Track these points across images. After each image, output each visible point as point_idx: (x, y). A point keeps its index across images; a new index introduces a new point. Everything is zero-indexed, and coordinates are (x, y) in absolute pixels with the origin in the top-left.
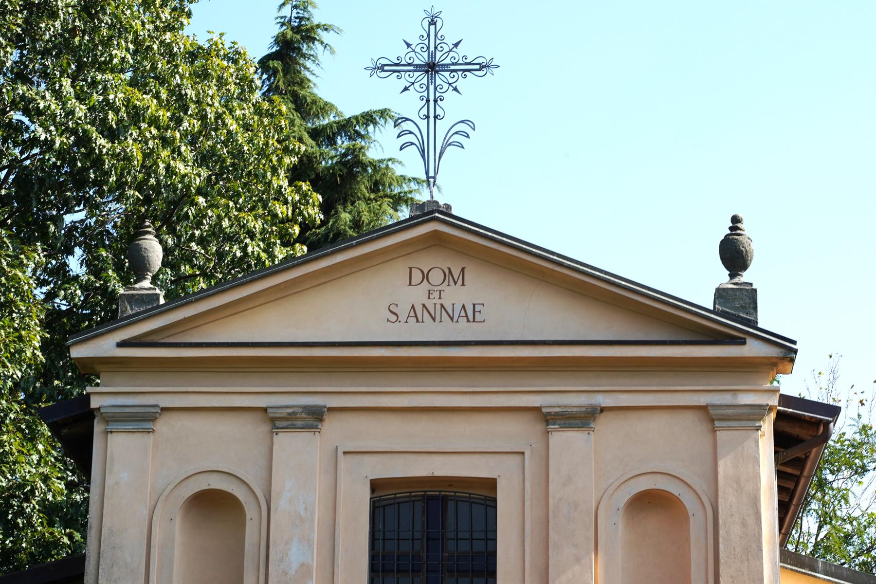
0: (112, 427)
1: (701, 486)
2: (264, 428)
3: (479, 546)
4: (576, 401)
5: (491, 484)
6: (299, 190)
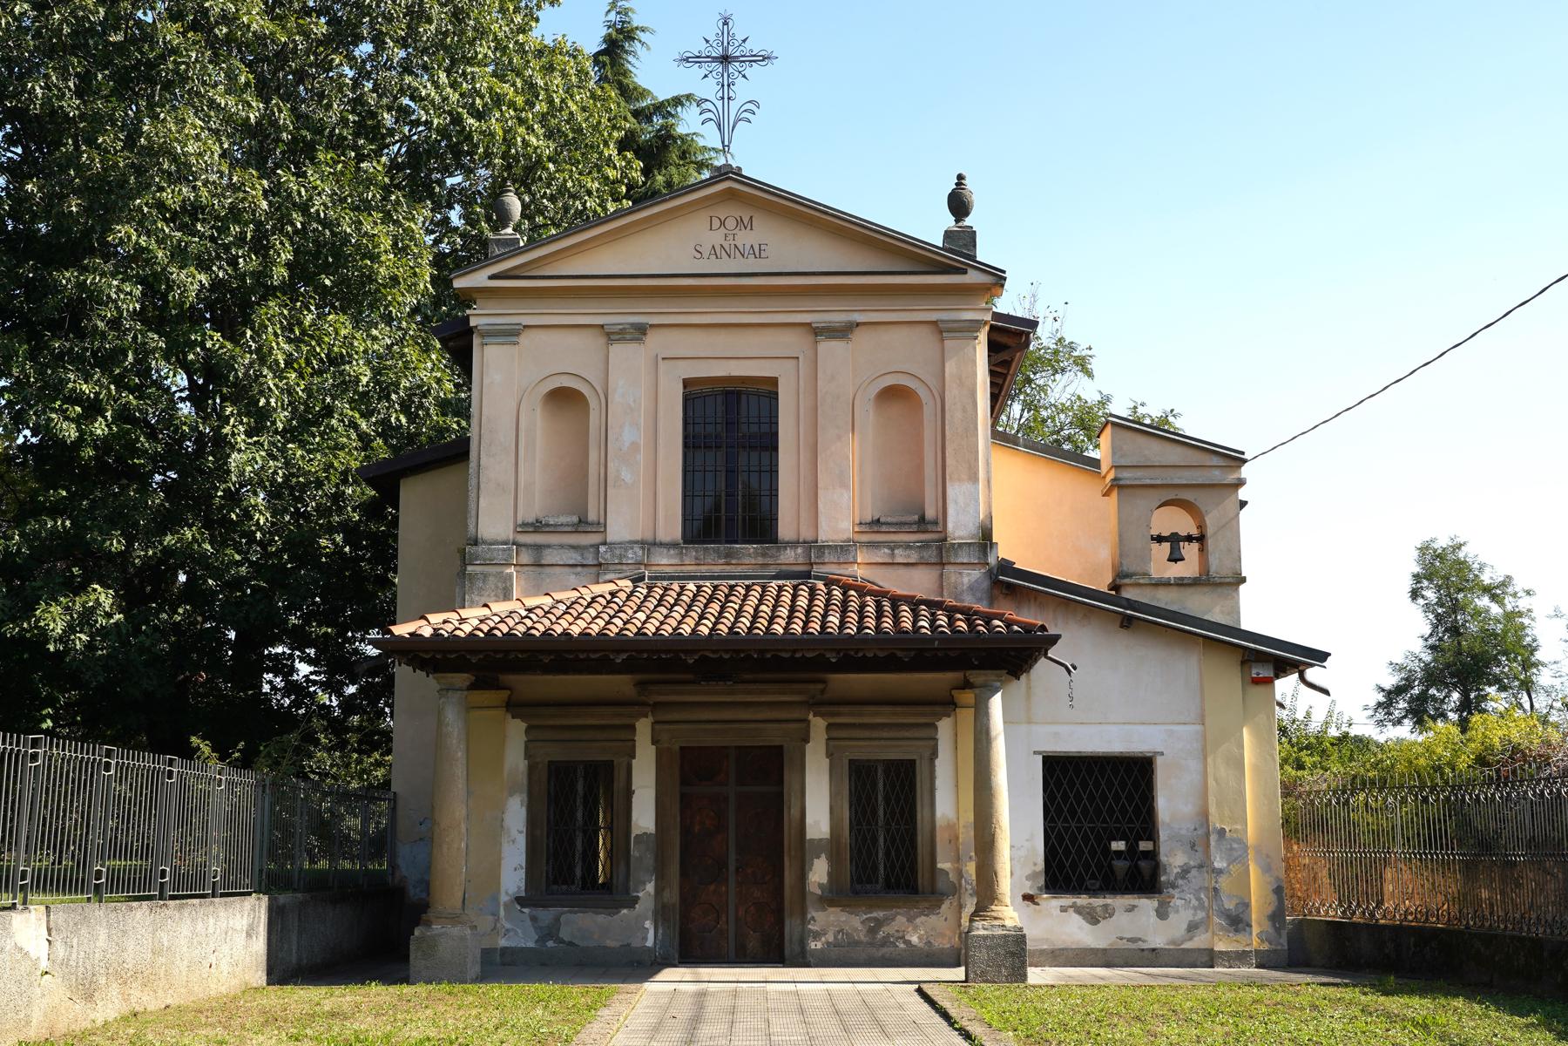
1: (932, 382)
3: (765, 428)
5: (774, 381)
6: (625, 158)
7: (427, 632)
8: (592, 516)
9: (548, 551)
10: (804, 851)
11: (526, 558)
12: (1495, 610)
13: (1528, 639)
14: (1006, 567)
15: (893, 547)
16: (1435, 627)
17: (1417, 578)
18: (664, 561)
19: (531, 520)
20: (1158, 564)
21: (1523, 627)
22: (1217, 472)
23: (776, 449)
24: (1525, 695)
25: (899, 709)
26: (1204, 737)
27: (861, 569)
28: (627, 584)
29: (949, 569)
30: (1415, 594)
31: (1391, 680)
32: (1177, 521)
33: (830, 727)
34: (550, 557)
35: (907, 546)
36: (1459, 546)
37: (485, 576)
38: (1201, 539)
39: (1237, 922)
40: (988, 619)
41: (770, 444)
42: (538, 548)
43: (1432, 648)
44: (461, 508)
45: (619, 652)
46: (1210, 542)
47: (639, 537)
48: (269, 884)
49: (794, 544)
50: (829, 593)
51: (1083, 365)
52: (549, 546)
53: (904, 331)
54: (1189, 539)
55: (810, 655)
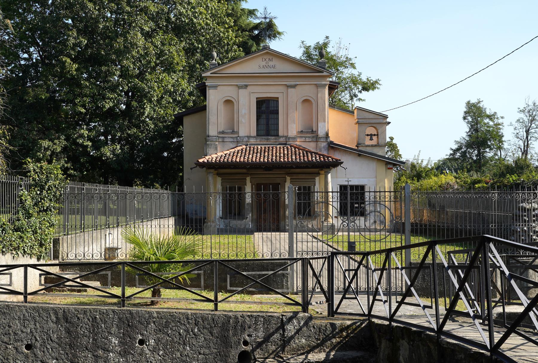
0: (210, 88)
1: (315, 98)
2: (237, 88)
3: (275, 109)
4: (293, 83)
5: (278, 98)
6: (229, 19)
7: (206, 161)
8: (235, 130)
9: (225, 139)
10: (285, 207)
11: (220, 140)
12: (491, 123)
13: (501, 133)
14: (332, 143)
15: (306, 137)
16: (470, 129)
17: (465, 112)
18: (252, 141)
19: (221, 131)
20: (368, 142)
21: (500, 129)
22: (381, 120)
23: (278, 113)
24: (499, 151)
25: (307, 175)
26: (376, 181)
27: (298, 142)
28: (244, 147)
29: (318, 143)
30: (465, 118)
31: (455, 147)
32: (372, 131)
33: (291, 179)
34: (226, 140)
35: (309, 137)
36: (479, 102)
37: (211, 144)
38: (378, 135)
39: (383, 222)
40: (328, 157)
41: (277, 113)
42: (223, 138)
43: (469, 136)
44: (204, 125)
45: (248, 165)
46: (379, 136)
47: (246, 135)
48: (173, 215)
49: (283, 137)
50: (291, 149)
51: (353, 66)
52: (226, 137)
53: (308, 86)
54: (375, 135)
55: (289, 166)
